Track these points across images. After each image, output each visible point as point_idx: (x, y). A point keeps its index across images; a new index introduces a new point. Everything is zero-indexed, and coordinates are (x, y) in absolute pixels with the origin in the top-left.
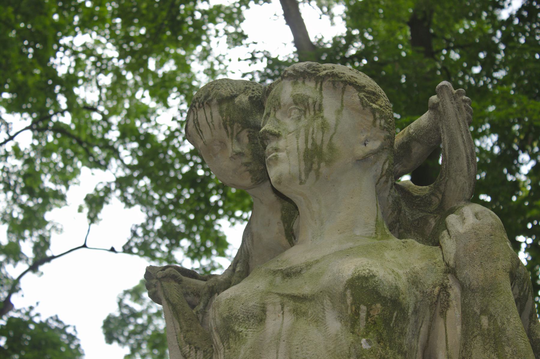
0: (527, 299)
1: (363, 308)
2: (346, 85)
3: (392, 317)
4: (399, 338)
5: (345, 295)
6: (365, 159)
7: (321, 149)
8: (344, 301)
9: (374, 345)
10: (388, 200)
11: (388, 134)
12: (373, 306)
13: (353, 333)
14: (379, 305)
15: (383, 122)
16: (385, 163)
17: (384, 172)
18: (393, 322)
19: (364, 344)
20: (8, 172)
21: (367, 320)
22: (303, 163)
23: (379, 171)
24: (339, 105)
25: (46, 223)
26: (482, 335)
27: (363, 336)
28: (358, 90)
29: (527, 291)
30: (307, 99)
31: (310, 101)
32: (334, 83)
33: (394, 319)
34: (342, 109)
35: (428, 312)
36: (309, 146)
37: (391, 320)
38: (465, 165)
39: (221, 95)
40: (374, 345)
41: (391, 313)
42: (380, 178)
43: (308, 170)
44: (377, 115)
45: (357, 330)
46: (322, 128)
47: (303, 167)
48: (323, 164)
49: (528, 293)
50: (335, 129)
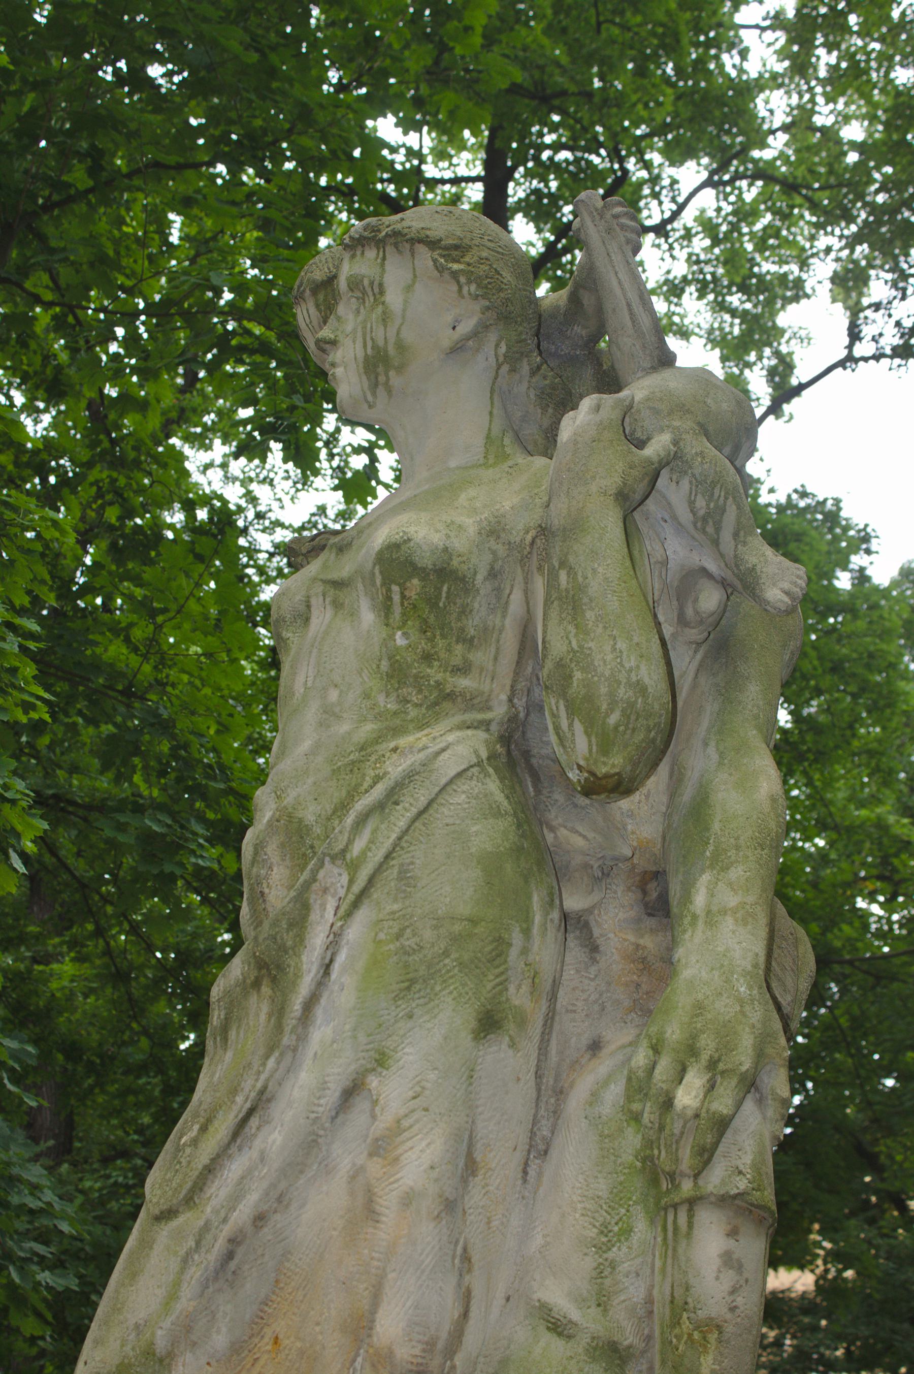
0: (724, 511)
1: (395, 588)
2: (413, 244)
3: (440, 594)
4: (459, 619)
5: (374, 574)
6: (456, 349)
7: (386, 351)
8: (373, 583)
9: (413, 638)
10: (528, 396)
11: (488, 303)
12: (408, 584)
13: (387, 625)
14: (415, 581)
15: (473, 287)
16: (497, 346)
17: (501, 359)
18: (443, 599)
19: (400, 640)
20: (698, 262)
21: (402, 604)
22: (364, 377)
23: (492, 360)
24: (410, 276)
25: (782, 332)
26: (560, 599)
27: (399, 628)
28: (430, 249)
29: (722, 498)
30: (362, 281)
31: (366, 282)
32: (396, 245)
33: (444, 595)
34: (414, 282)
35: (519, 570)
36: (369, 351)
37: (438, 597)
38: (628, 318)
39: (314, 281)
40: (413, 638)
41: (439, 590)
42: (498, 369)
43: (374, 386)
44: (463, 280)
45: (391, 621)
46: (384, 320)
47: (366, 384)
48: (392, 373)
49: (725, 502)
50: (403, 317)
